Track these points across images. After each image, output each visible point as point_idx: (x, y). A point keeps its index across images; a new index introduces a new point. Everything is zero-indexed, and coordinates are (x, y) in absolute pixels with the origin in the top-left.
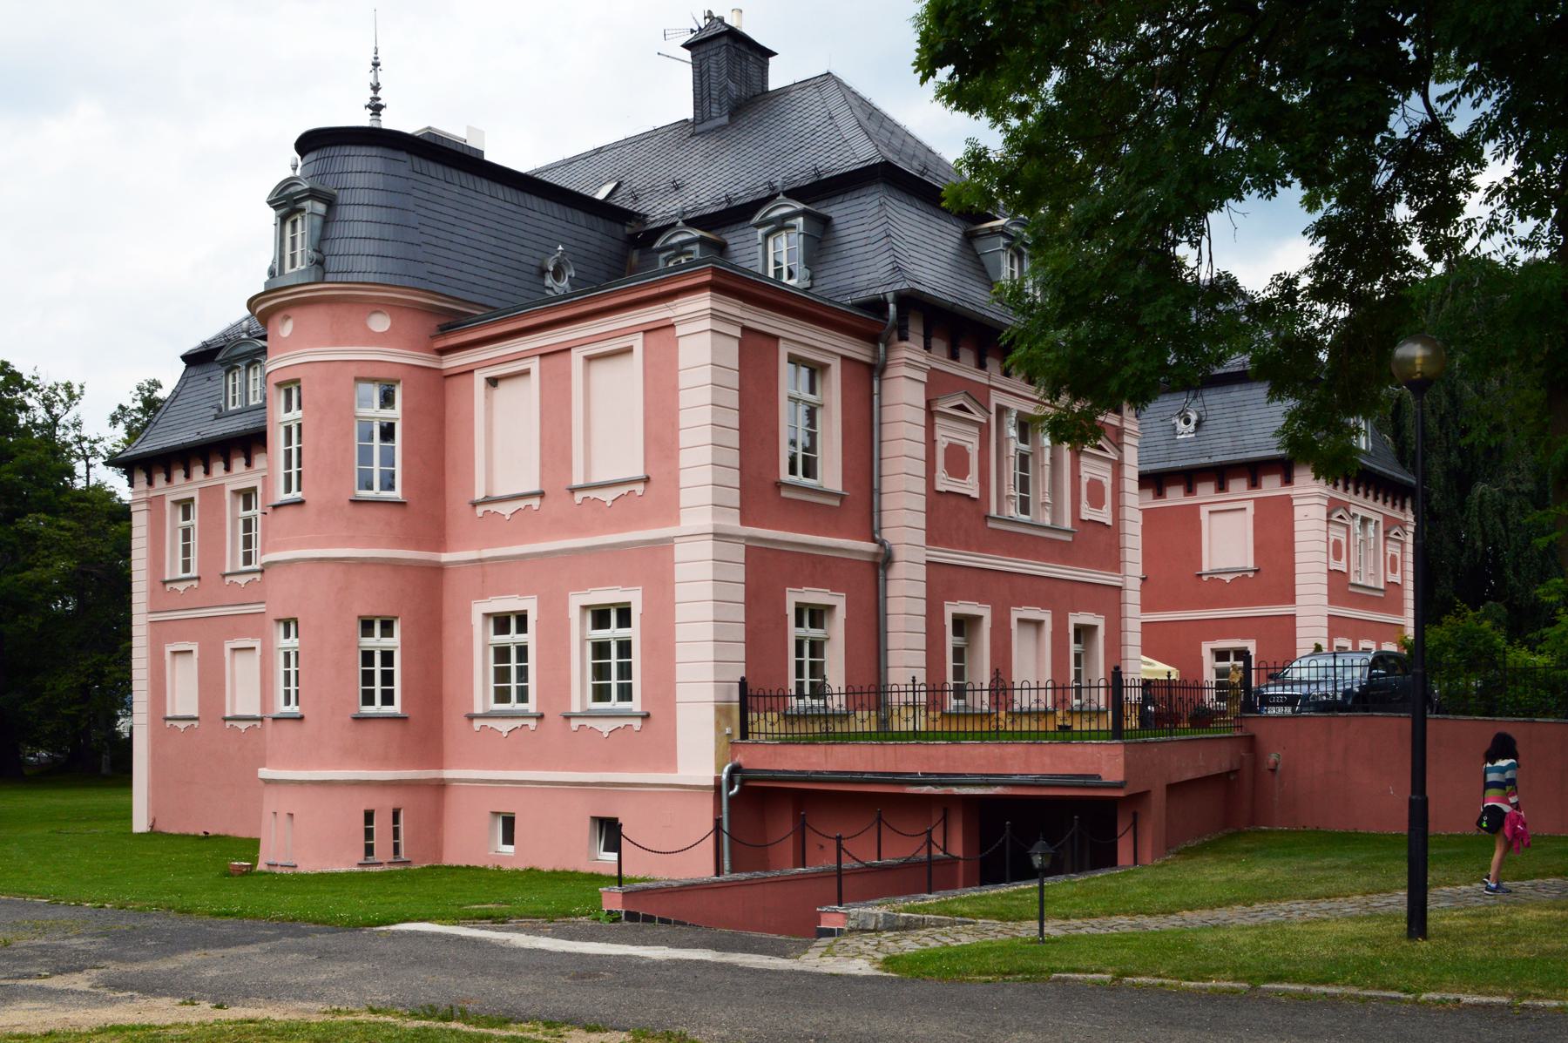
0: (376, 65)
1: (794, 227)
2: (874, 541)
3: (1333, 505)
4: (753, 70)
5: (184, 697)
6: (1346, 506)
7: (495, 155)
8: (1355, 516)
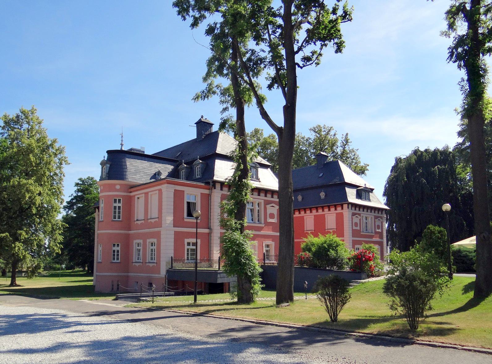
7: (147, 153)
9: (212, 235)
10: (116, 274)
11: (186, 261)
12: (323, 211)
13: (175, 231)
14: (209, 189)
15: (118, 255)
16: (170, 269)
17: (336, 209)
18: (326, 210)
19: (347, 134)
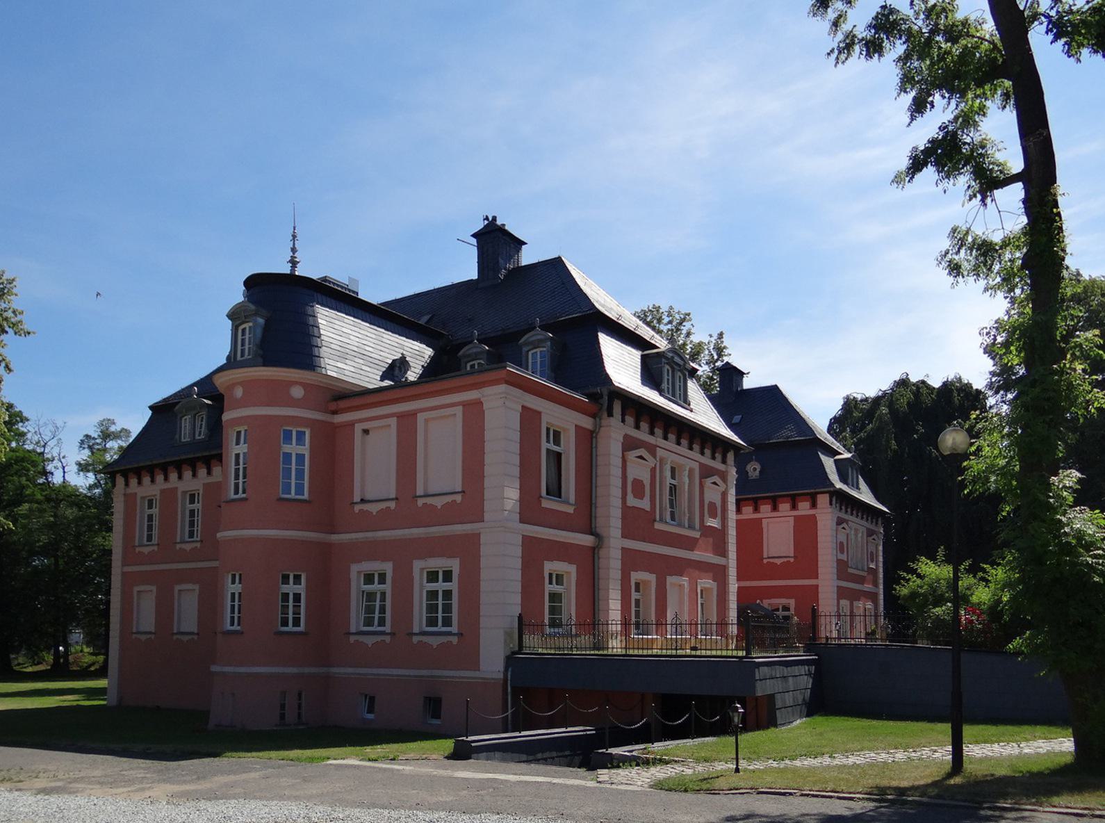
0: (294, 237)
2: (592, 534)
3: (840, 522)
5: (146, 619)
6: (846, 521)
9: (602, 553)
10: (313, 670)
11: (548, 630)
12: (756, 510)
13: (524, 537)
14: (594, 416)
15: (447, 609)
16: (514, 653)
17: (794, 507)
18: (765, 509)
19: (721, 335)
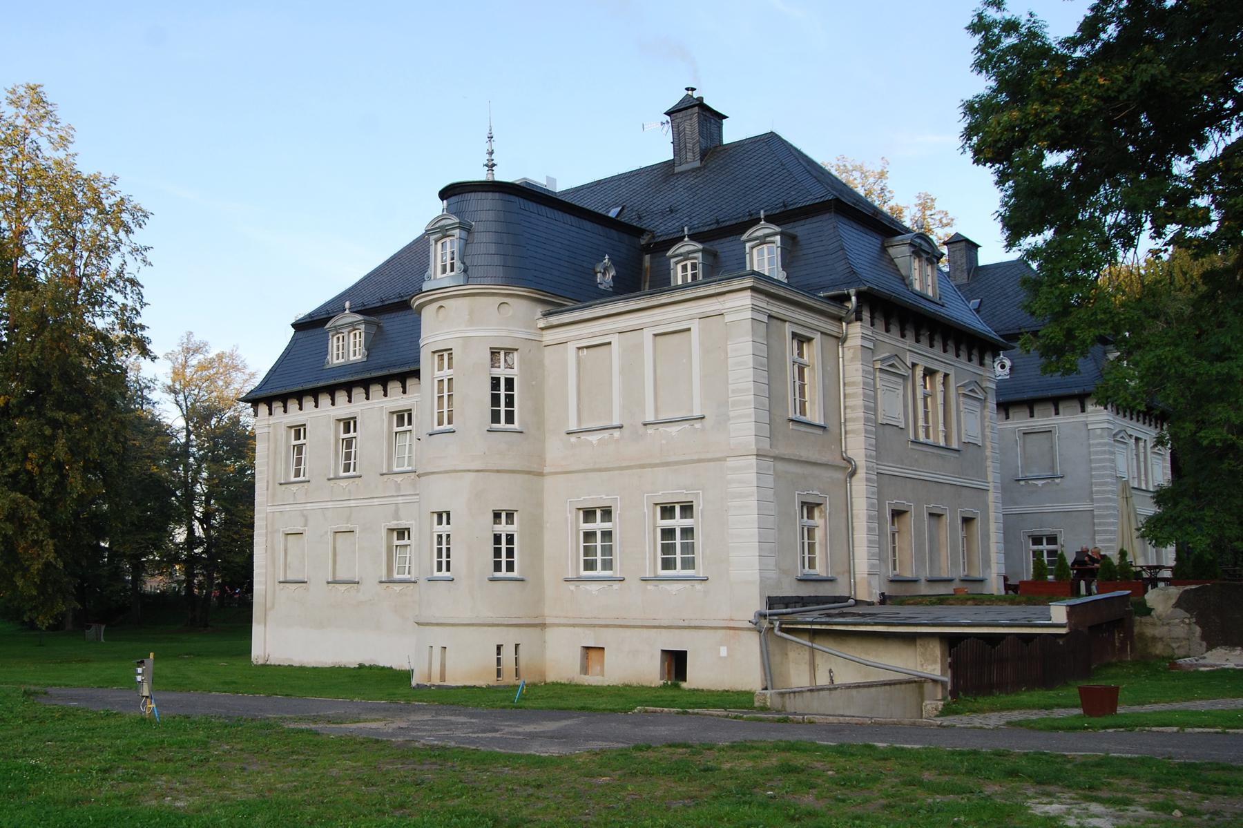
1: (773, 242)
4: (714, 128)
8: (1131, 436)
